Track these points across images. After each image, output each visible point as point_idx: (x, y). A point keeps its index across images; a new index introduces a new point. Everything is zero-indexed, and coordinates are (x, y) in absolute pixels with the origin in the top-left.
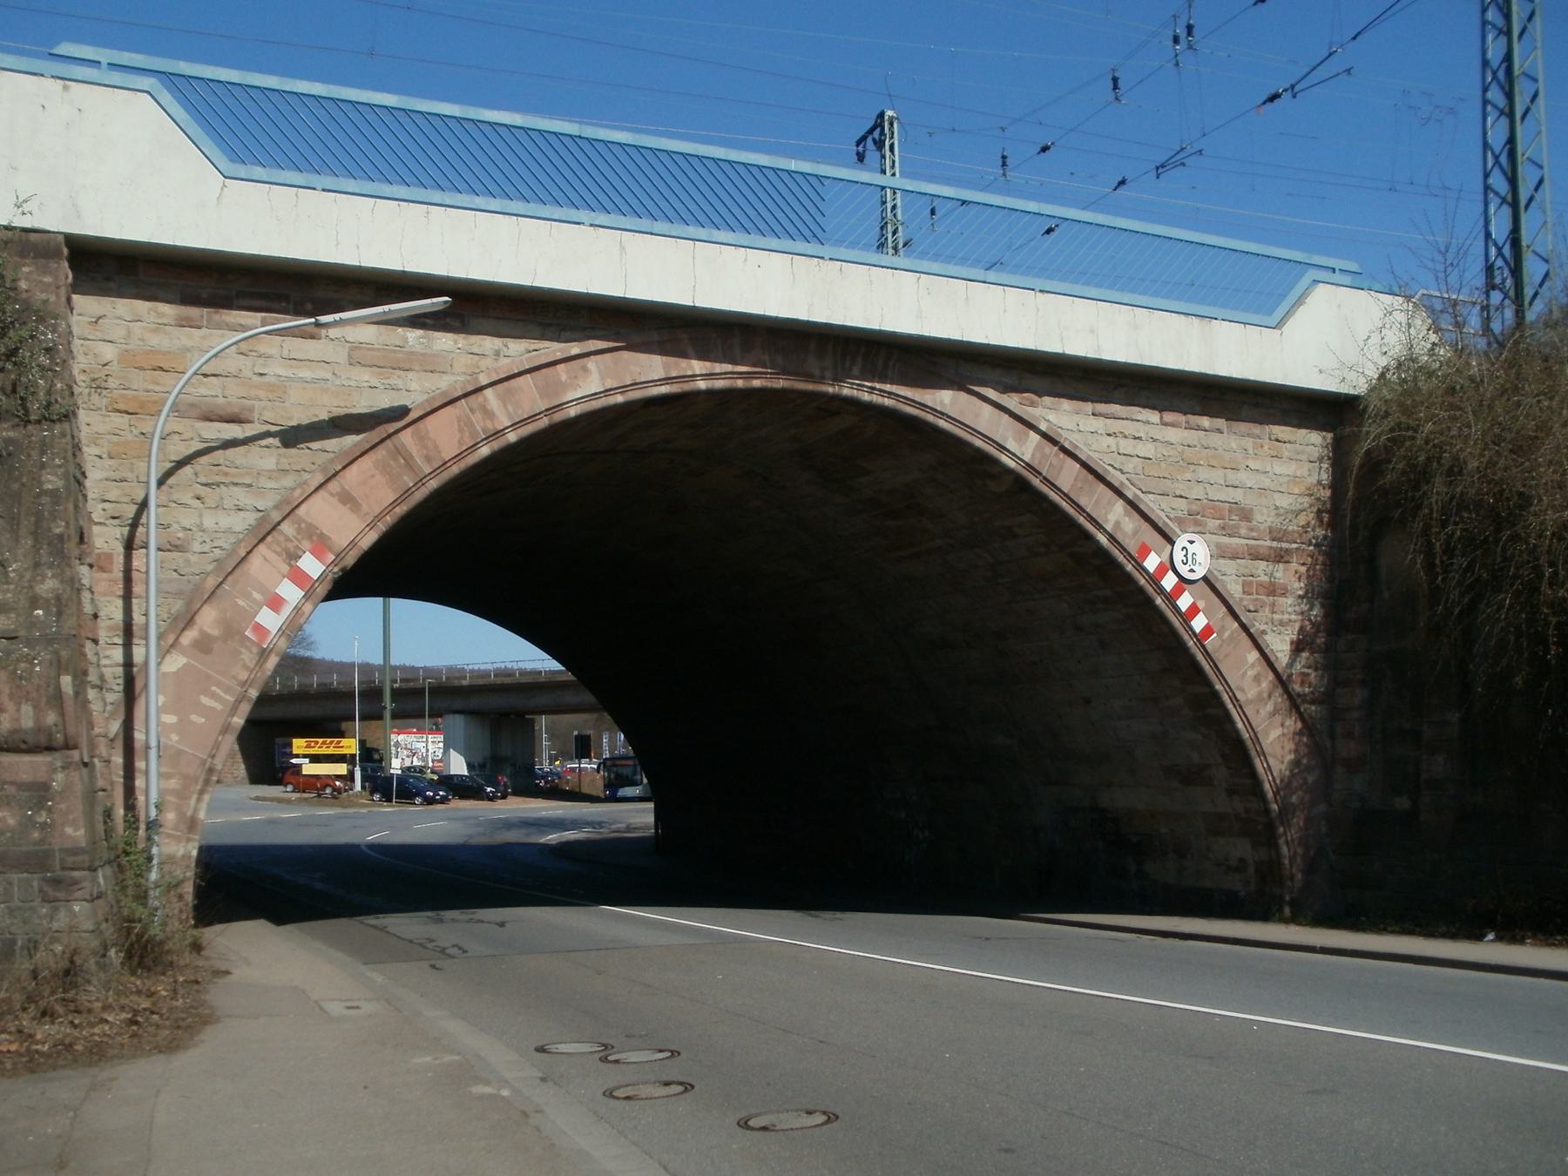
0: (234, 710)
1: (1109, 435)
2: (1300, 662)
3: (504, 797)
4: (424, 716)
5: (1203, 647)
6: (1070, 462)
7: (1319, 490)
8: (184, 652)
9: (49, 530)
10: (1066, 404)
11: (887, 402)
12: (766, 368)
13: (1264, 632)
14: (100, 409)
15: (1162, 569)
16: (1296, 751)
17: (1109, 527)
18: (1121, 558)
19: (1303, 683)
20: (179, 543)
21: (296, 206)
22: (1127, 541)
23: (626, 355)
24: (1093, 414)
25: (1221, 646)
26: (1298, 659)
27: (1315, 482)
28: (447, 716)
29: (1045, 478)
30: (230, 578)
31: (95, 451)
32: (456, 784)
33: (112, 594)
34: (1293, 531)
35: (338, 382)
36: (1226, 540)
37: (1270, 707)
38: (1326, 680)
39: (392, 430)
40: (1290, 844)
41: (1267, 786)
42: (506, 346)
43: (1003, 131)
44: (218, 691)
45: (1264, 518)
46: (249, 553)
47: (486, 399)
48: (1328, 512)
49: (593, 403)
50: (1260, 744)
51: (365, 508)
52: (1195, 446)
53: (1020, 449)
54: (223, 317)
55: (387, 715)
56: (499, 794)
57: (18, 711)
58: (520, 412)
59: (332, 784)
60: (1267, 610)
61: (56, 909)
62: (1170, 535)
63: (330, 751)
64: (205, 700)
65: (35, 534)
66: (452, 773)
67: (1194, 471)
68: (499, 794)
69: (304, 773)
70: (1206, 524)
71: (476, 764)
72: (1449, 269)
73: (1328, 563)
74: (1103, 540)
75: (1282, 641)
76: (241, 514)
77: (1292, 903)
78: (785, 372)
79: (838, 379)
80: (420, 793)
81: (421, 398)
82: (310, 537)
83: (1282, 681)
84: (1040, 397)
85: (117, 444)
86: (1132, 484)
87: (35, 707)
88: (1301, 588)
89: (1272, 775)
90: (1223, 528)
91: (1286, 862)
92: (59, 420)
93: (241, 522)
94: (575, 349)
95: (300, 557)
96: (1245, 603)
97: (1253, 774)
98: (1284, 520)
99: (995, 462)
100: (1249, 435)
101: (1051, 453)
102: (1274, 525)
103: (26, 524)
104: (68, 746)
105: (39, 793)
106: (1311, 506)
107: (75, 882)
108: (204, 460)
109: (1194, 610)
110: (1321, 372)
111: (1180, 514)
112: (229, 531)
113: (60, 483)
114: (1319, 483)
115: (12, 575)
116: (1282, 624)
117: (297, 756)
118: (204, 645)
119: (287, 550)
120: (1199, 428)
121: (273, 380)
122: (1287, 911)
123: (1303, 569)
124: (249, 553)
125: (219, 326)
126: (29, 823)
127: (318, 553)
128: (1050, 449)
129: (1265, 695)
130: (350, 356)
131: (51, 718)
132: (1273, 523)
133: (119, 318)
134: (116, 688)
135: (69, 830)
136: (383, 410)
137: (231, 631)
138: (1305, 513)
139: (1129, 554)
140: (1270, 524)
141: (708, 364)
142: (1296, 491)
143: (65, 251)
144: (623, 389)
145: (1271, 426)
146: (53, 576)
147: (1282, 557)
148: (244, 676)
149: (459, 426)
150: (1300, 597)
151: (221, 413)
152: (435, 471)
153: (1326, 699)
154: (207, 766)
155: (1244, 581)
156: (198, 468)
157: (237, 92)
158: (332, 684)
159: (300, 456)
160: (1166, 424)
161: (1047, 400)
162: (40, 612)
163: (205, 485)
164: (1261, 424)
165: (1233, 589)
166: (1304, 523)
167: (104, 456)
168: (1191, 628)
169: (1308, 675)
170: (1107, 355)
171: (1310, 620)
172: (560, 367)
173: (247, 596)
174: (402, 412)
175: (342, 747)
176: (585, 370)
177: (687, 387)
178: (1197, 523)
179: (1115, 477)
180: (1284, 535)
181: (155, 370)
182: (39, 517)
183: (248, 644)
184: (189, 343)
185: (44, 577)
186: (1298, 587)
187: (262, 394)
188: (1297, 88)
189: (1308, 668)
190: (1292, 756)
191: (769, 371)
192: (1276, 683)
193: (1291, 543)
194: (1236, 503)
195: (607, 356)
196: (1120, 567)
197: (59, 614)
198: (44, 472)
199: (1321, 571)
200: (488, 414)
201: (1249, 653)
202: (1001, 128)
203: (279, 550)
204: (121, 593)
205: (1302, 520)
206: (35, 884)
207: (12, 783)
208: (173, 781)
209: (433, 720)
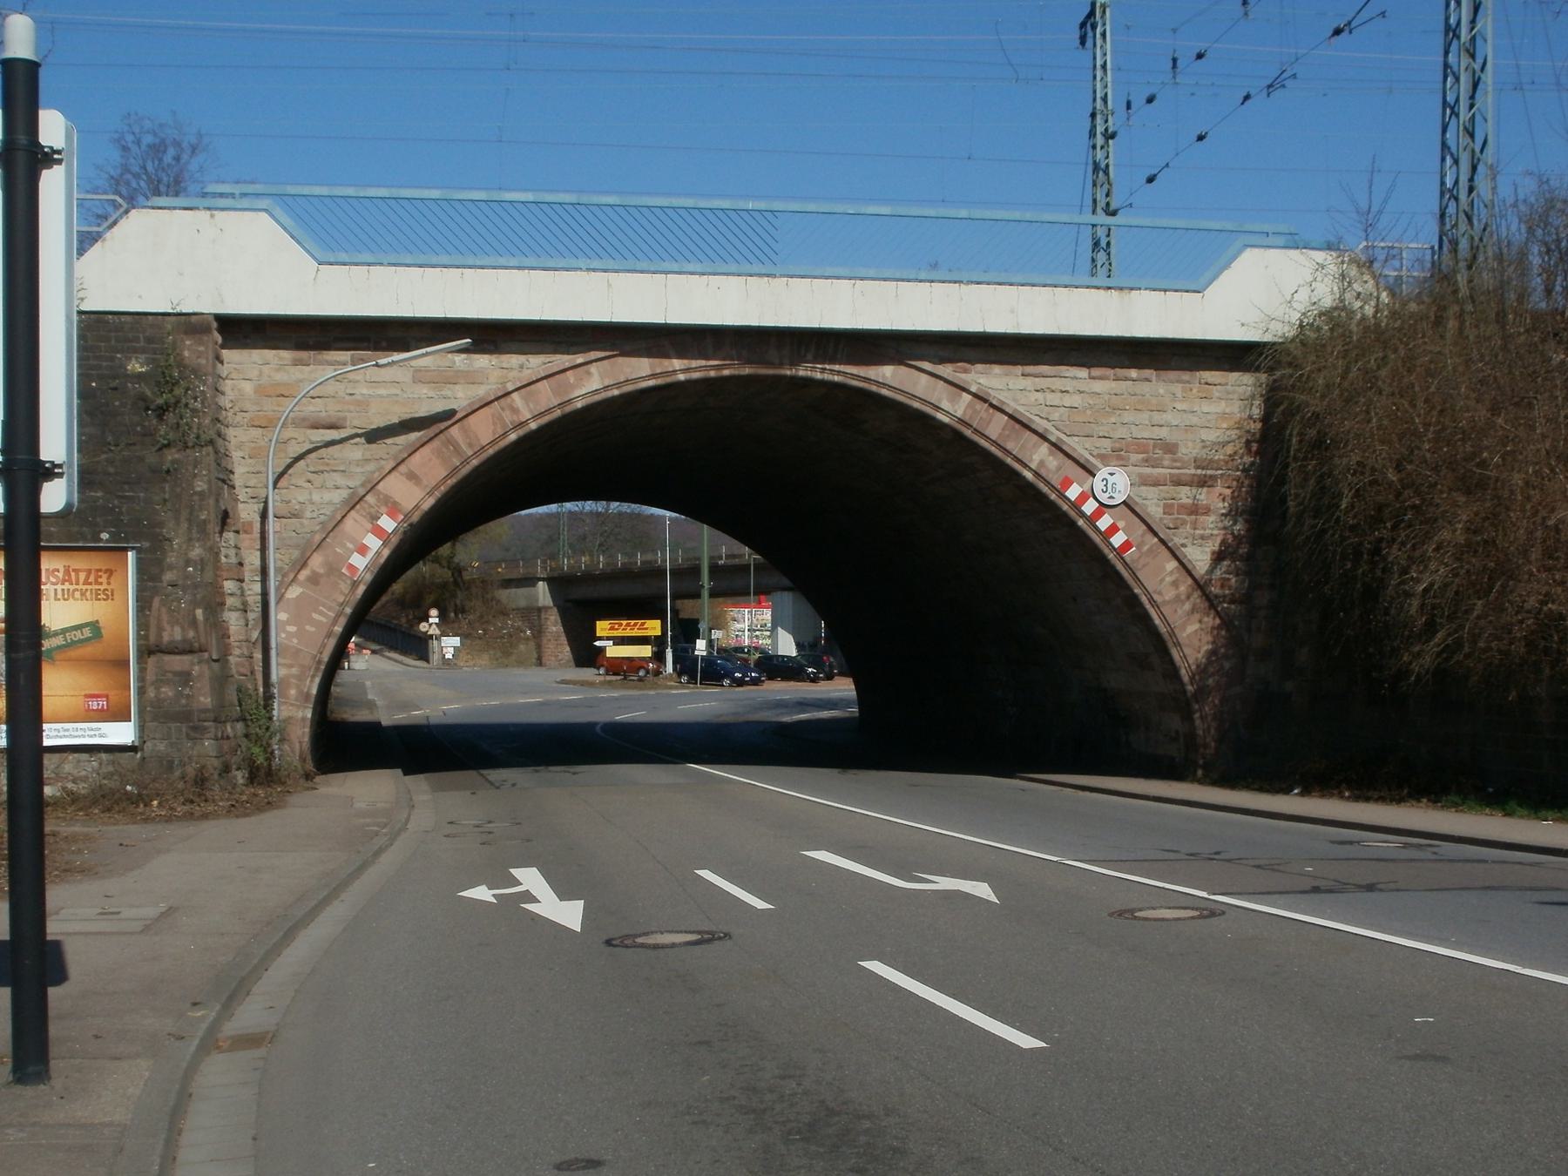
0: (335, 622)
1: (1037, 391)
2: (1221, 569)
3: (830, 677)
4: (749, 594)
5: (1122, 558)
6: (998, 414)
7: (1249, 424)
8: (301, 585)
9: (198, 516)
10: (997, 369)
11: (836, 378)
12: (734, 360)
13: (1184, 545)
14: (243, 426)
15: (1083, 498)
16: (1213, 642)
17: (1033, 466)
18: (1045, 489)
19: (1222, 586)
20: (296, 512)
21: (368, 279)
22: (1050, 476)
23: (620, 360)
24: (1023, 375)
25: (1140, 557)
26: (1219, 567)
27: (1246, 417)
28: (774, 594)
29: (975, 429)
30: (331, 534)
31: (240, 454)
32: (776, 665)
33: (252, 548)
34: (1219, 460)
35: (405, 396)
36: (1148, 470)
37: (1187, 606)
38: (1246, 585)
39: (443, 428)
40: (1204, 722)
41: (1183, 672)
42: (528, 361)
43: (1175, 32)
44: (324, 610)
45: (1189, 450)
46: (343, 517)
47: (513, 400)
48: (1257, 442)
49: (596, 396)
50: (1175, 636)
51: (425, 482)
52: (1122, 394)
53: (951, 408)
54: (324, 356)
55: (705, 593)
56: (821, 675)
57: (172, 630)
58: (538, 408)
59: (646, 666)
60: (1188, 527)
61: (195, 744)
62: (1091, 469)
63: (636, 633)
64: (315, 616)
65: (189, 520)
66: (779, 654)
67: (1119, 415)
68: (821, 675)
69: (608, 656)
70: (1129, 459)
71: (806, 644)
72: (1369, 229)
73: (1255, 485)
74: (1029, 475)
75: (1202, 552)
76: (338, 490)
77: (1204, 767)
78: (749, 362)
79: (794, 363)
80: (729, 675)
81: (465, 403)
82: (386, 505)
83: (1200, 586)
84: (973, 365)
85: (254, 448)
86: (1057, 429)
87: (182, 628)
88: (1224, 507)
89: (1188, 662)
90: (1147, 461)
91: (1201, 732)
92: (206, 445)
93: (338, 496)
94: (580, 359)
95: (379, 518)
96: (1165, 521)
97: (1171, 661)
98: (1210, 451)
99: (934, 419)
100: (1178, 381)
101: (981, 409)
102: (1199, 456)
103: (184, 514)
104: (201, 650)
105: (185, 677)
106: (1239, 438)
107: (206, 728)
108: (313, 455)
109: (1113, 529)
110: (1243, 325)
111: (1103, 451)
112: (330, 503)
113: (205, 487)
114: (1250, 417)
115: (175, 546)
116: (1202, 537)
117: (600, 639)
118: (314, 580)
119: (369, 513)
120: (1126, 379)
121: (359, 397)
122: (1200, 772)
123: (1228, 492)
124: (343, 517)
125: (321, 363)
126: (179, 695)
127: (392, 515)
128: (979, 405)
129: (1183, 597)
130: (413, 376)
131: (191, 634)
132: (1198, 454)
133: (255, 363)
134: (256, 609)
135: (202, 699)
136: (438, 413)
137: (333, 569)
138: (1233, 444)
139: (1053, 486)
140: (1195, 455)
141: (686, 361)
142: (1225, 426)
143: (215, 325)
144: (618, 385)
145: (1201, 372)
146: (199, 546)
147: (1205, 482)
148: (341, 599)
149: (493, 421)
150: (1223, 515)
151: (324, 423)
152: (476, 453)
153: (1245, 599)
154: (317, 659)
155: (1164, 504)
156: (309, 461)
157: (327, 201)
158: (656, 562)
159: (379, 449)
160: (1094, 378)
161: (979, 367)
162: (191, 569)
163: (314, 472)
164: (1191, 371)
165: (1154, 510)
166: (1231, 452)
167: (246, 457)
168: (1111, 544)
169: (1229, 579)
170: (1026, 329)
171: (1233, 534)
172: (569, 373)
173: (343, 546)
174: (452, 413)
175: (646, 629)
176: (589, 373)
177: (669, 380)
178: (1120, 458)
179: (1040, 424)
180: (1209, 463)
181: (278, 396)
182: (192, 509)
183: (344, 578)
184: (300, 376)
185: (194, 546)
186: (1222, 507)
187: (352, 408)
188: (1353, 25)
189: (1229, 574)
190: (1210, 647)
191: (736, 362)
192: (1196, 587)
193: (1217, 470)
194: (1161, 439)
195: (605, 362)
196: (1045, 496)
197: (202, 570)
198: (195, 480)
199: (1247, 492)
200: (515, 410)
201: (1168, 562)
202: (1173, 29)
203: (364, 514)
204: (259, 547)
205: (1229, 449)
206: (184, 730)
207: (170, 672)
208: (294, 669)
209: (757, 597)
